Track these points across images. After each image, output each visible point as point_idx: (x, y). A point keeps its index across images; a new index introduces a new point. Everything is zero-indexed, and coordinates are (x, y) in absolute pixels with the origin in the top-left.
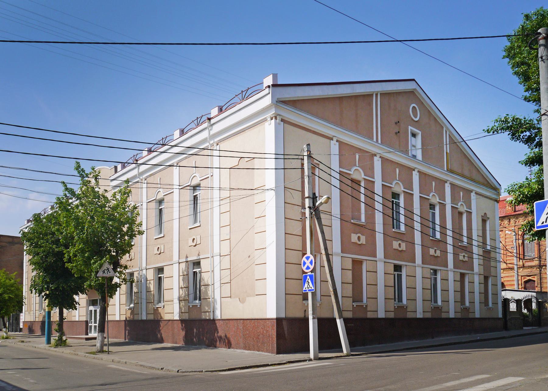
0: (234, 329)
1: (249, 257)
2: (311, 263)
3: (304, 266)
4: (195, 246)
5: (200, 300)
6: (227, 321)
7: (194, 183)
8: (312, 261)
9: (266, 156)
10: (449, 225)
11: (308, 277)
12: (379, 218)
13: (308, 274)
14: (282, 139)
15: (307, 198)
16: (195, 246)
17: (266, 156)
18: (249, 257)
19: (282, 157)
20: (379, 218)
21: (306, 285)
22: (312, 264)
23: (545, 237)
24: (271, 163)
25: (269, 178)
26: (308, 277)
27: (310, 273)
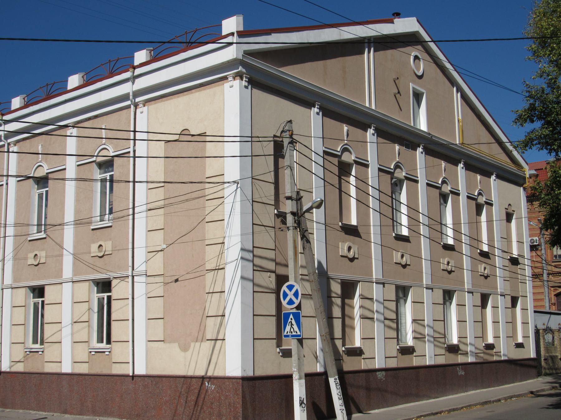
0: (169, 392)
1: (177, 281)
2: (285, 295)
3: (284, 299)
4: (36, 266)
5: (109, 342)
6: (158, 379)
7: (40, 173)
8: (297, 292)
9: (226, 139)
10: (464, 229)
11: (291, 316)
12: (373, 218)
13: (291, 311)
14: (251, 114)
15: (71, 180)
16: (36, 266)
17: (226, 139)
18: (177, 281)
19: (250, 139)
20: (373, 218)
21: (288, 328)
22: (297, 298)
23: (281, 356)
24: (234, 149)
25: (232, 169)
26: (291, 316)
27: (295, 311)
